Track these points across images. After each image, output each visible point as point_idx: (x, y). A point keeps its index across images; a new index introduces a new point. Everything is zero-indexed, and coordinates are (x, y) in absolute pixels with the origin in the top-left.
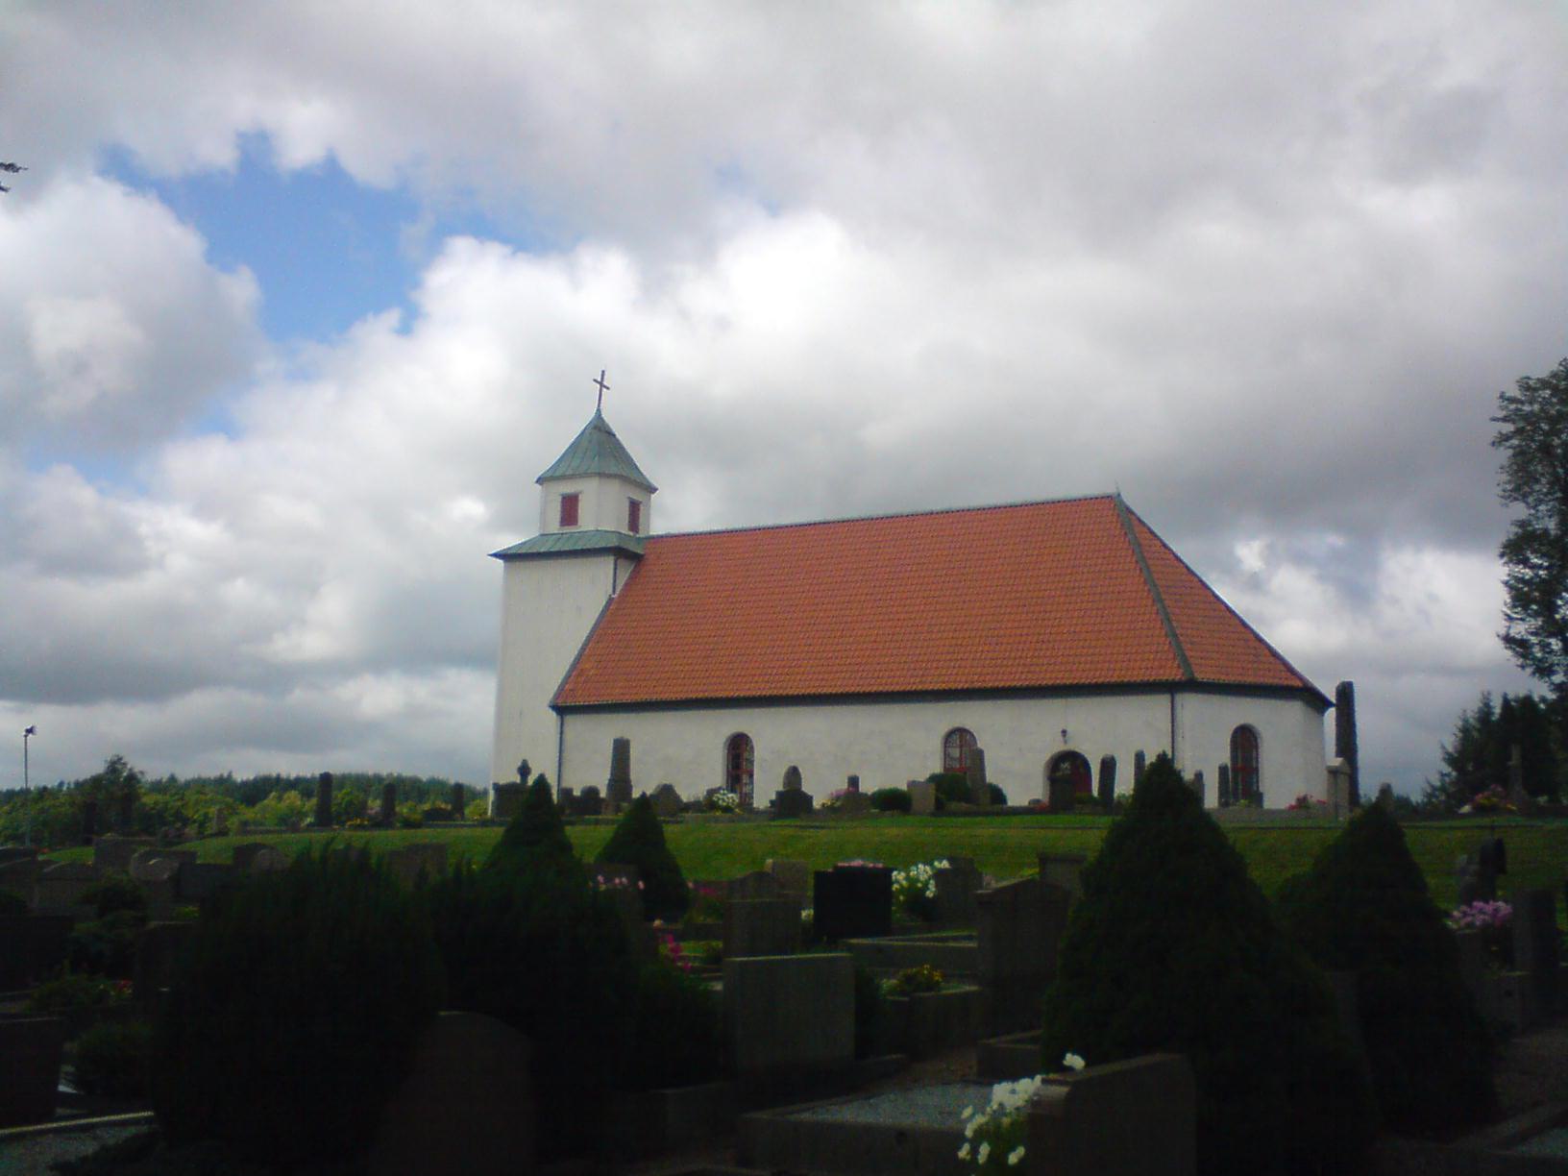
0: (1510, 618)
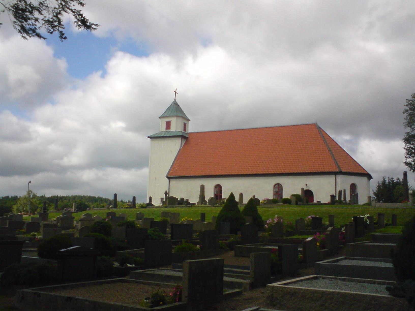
0: (406, 157)
